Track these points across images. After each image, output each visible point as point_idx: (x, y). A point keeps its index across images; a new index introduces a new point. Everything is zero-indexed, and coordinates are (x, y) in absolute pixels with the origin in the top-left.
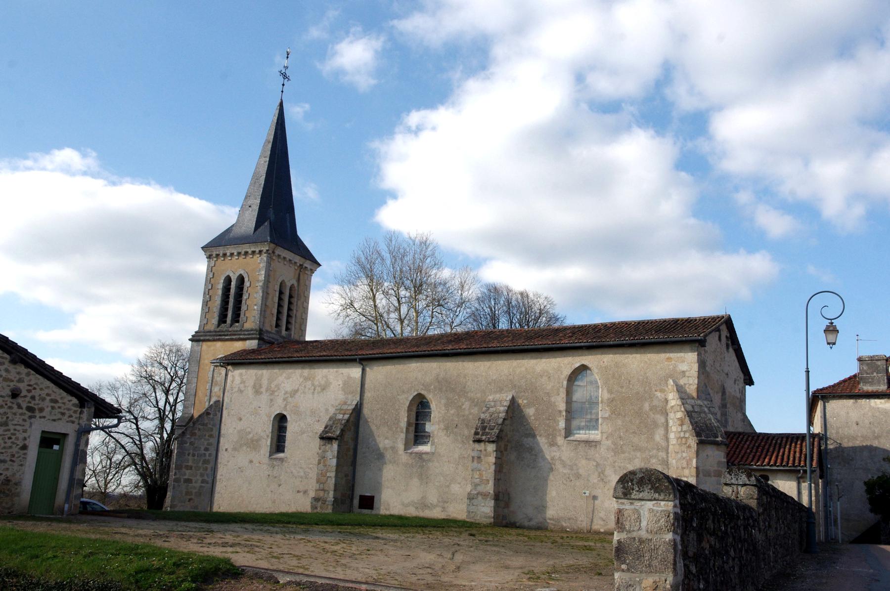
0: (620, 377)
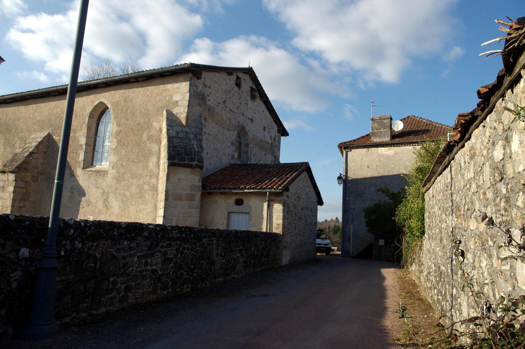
0: (127, 110)
